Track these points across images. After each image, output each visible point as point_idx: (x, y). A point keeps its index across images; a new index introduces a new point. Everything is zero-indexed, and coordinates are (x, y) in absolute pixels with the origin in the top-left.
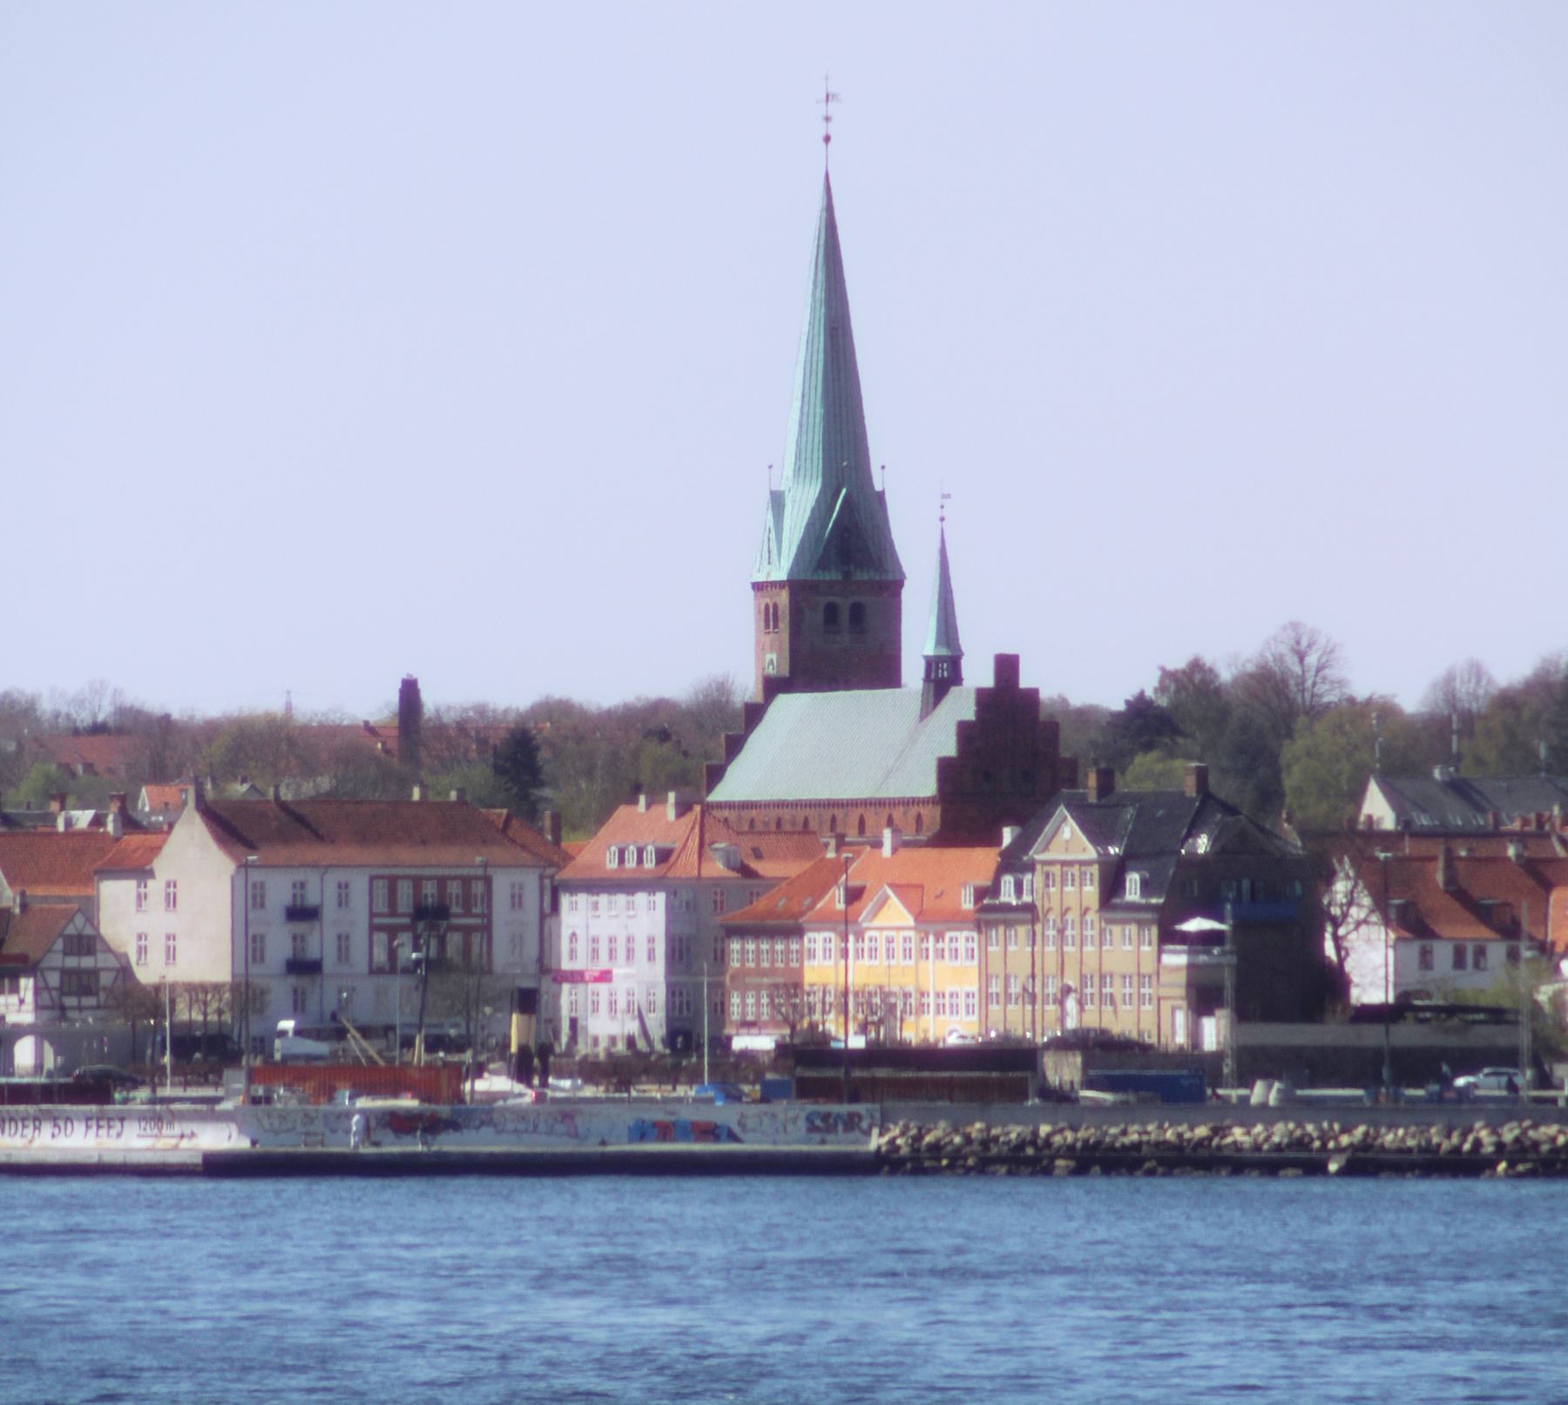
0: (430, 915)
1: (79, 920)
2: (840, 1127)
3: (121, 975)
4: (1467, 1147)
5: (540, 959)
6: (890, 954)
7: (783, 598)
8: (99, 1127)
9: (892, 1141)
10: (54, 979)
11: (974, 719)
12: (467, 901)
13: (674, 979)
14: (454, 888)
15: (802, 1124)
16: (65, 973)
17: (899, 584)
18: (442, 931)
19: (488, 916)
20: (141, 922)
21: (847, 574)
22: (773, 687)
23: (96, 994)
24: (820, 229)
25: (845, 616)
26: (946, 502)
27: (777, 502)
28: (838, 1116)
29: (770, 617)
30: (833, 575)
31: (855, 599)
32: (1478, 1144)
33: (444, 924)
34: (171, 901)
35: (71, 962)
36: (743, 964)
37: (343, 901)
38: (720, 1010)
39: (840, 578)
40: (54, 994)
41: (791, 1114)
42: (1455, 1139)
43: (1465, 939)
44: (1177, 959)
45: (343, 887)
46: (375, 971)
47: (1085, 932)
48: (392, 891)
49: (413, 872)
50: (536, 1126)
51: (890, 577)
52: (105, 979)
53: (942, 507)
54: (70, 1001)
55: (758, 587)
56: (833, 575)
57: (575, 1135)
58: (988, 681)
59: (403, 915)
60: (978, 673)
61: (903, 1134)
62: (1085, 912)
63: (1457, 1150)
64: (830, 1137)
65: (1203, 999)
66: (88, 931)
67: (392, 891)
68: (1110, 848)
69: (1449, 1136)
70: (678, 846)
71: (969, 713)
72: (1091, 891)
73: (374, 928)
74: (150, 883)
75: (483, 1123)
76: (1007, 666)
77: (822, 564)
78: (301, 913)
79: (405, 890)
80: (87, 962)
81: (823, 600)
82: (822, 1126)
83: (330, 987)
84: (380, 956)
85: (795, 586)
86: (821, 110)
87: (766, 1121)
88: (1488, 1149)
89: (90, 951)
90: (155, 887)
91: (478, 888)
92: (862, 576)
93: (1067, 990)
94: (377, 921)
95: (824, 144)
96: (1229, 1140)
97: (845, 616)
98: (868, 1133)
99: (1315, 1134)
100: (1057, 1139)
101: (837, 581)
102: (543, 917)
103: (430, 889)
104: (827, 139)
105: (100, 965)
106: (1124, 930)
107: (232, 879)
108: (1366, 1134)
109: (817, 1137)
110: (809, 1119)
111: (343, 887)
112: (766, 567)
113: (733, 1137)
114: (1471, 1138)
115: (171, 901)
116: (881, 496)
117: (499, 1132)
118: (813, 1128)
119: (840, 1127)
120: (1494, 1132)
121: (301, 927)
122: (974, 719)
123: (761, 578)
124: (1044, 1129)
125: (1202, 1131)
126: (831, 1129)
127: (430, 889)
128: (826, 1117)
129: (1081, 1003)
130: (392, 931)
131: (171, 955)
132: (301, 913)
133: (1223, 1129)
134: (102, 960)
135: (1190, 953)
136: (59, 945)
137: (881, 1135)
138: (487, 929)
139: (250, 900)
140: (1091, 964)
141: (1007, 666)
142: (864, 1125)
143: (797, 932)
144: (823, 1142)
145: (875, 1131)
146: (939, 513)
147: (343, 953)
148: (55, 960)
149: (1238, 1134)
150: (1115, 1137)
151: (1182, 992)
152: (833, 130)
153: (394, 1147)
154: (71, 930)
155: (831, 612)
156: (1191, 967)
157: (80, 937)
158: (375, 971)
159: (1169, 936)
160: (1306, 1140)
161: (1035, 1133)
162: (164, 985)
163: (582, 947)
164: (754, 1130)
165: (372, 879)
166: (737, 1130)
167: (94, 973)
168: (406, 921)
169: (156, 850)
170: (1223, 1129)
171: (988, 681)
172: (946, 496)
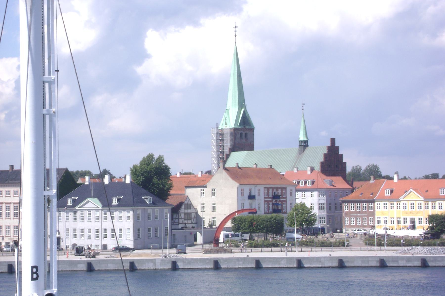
3: (196, 214)
6: (412, 207)
11: (340, 153)
13: (328, 214)
16: (185, 214)
17: (254, 129)
19: (286, 198)
20: (202, 200)
21: (244, 127)
23: (191, 220)
24: (235, 53)
26: (303, 105)
31: (246, 132)
33: (279, 200)
34: (213, 194)
38: (191, 207)
39: (243, 127)
40: (183, 219)
43: (2, 217)
45: (259, 190)
47: (265, 205)
51: (252, 128)
52: (193, 215)
53: (303, 107)
54: (186, 222)
59: (270, 198)
73: (265, 201)
79: (271, 191)
80: (189, 211)
81: (240, 132)
86: (234, 29)
90: (208, 190)
92: (247, 127)
94: (266, 199)
95: (235, 37)
97: (244, 135)
101: (243, 128)
104: (236, 36)
107: (238, 188)
111: (259, 190)
115: (213, 194)
122: (340, 153)
131: (214, 209)
132: (251, 197)
138: (286, 201)
139: (241, 193)
143: (373, 202)
146: (302, 108)
152: (237, 33)
153: (18, 216)
160: (223, 247)
162: (342, 211)
163: (125, 219)
165: (265, 188)
167: (190, 214)
168: (271, 199)
172: (303, 104)
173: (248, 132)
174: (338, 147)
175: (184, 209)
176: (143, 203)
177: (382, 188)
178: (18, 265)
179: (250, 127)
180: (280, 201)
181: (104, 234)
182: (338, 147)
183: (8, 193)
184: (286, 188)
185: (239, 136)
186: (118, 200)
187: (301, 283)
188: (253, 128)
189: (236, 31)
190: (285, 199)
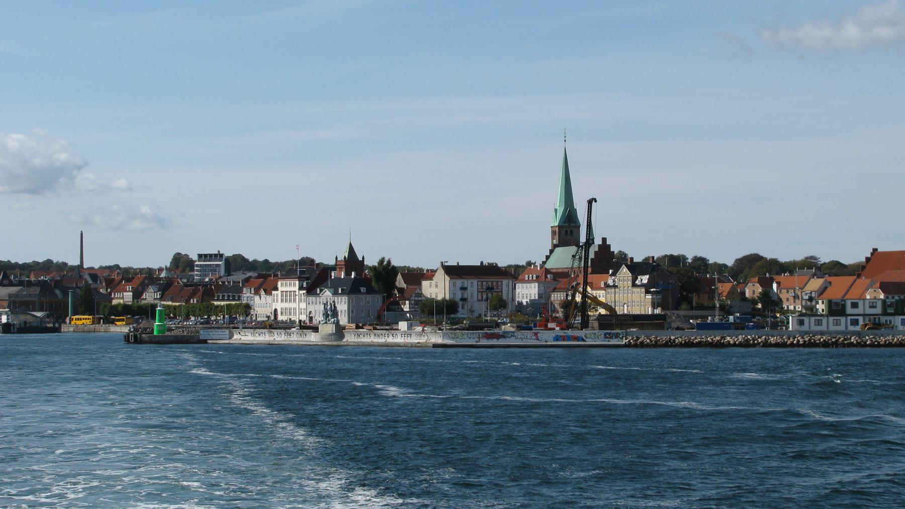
0: (490, 289)
1: (418, 290)
2: (614, 337)
4: (795, 342)
5: (512, 298)
7: (557, 229)
8: (408, 337)
9: (630, 341)
10: (413, 302)
12: (497, 285)
14: (495, 283)
15: (603, 336)
16: (415, 301)
18: (753, 320)
19: (502, 289)
22: (555, 246)
25: (569, 232)
27: (556, 210)
28: (613, 334)
29: (554, 233)
30: (567, 225)
31: (571, 229)
32: (798, 341)
35: (417, 299)
36: (567, 298)
37: (472, 286)
41: (600, 333)
42: (791, 340)
44: (649, 297)
46: (478, 300)
48: (482, 283)
49: (496, 280)
50: (527, 337)
51: (578, 225)
55: (552, 227)
56: (567, 225)
57: (537, 339)
58: (601, 243)
60: (598, 241)
61: (632, 339)
62: (628, 287)
63: (792, 343)
64: (611, 340)
65: (654, 306)
66: (420, 292)
67: (482, 283)
68: (648, 276)
69: (789, 339)
70: (540, 275)
71: (597, 249)
72: (630, 283)
73: (478, 292)
74: (461, 286)
75: (512, 336)
76: (604, 240)
77: (565, 222)
78: (463, 289)
80: (420, 299)
82: (608, 336)
83: (469, 304)
84: (480, 298)
85: (559, 227)
87: (593, 335)
88: (801, 343)
89: (421, 297)
90: (433, 282)
91: (500, 283)
92: (572, 225)
93: (625, 304)
96: (726, 340)
97: (569, 232)
98: (622, 339)
99: (751, 339)
100: (677, 341)
102: (513, 289)
103: (490, 283)
104: (565, 141)
105: (423, 299)
106: (846, 320)
108: (766, 338)
109: (607, 340)
110: (605, 334)
112: (554, 223)
113: (584, 340)
114: (796, 339)
115: (437, 286)
116: (737, 261)
117: (516, 339)
118: (606, 337)
119: (614, 337)
120: (802, 338)
121: (463, 292)
123: (552, 225)
124: (673, 338)
125: (718, 338)
126: (611, 338)
127: (490, 283)
128: (610, 334)
129: (628, 306)
130: (482, 292)
132: (463, 289)
133: (724, 337)
134: (423, 298)
135: (652, 296)
136: (414, 295)
137: (626, 339)
138: (502, 292)
140: (630, 300)
141: (604, 240)
142: (621, 336)
144: (609, 341)
145: (624, 338)
147: (472, 296)
148: (413, 298)
149: (728, 338)
150: (694, 340)
151: (651, 304)
154: (416, 292)
155: (566, 232)
156: (652, 298)
157: (418, 293)
158: (478, 300)
159: (647, 292)
161: (670, 338)
164: (589, 338)
166: (584, 338)
169: (434, 275)
170: (724, 337)
171: (601, 243)
173: (573, 229)
174: (610, 245)
175: (643, 290)
176: (359, 292)
177: (173, 302)
178: (573, 350)
179: (575, 225)
180: (495, 292)
181: (290, 309)
182: (610, 245)
183: (290, 285)
184: (502, 282)
185: (563, 233)
186: (342, 290)
187: (732, 360)
188: (323, 267)
189: (565, 137)
190: (500, 290)
